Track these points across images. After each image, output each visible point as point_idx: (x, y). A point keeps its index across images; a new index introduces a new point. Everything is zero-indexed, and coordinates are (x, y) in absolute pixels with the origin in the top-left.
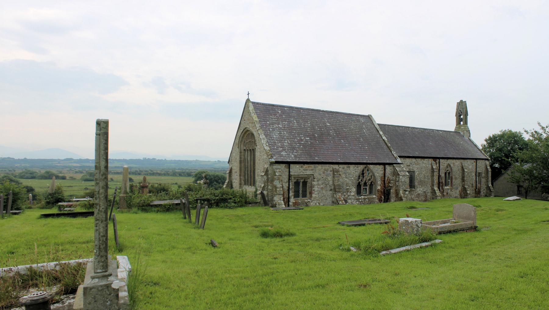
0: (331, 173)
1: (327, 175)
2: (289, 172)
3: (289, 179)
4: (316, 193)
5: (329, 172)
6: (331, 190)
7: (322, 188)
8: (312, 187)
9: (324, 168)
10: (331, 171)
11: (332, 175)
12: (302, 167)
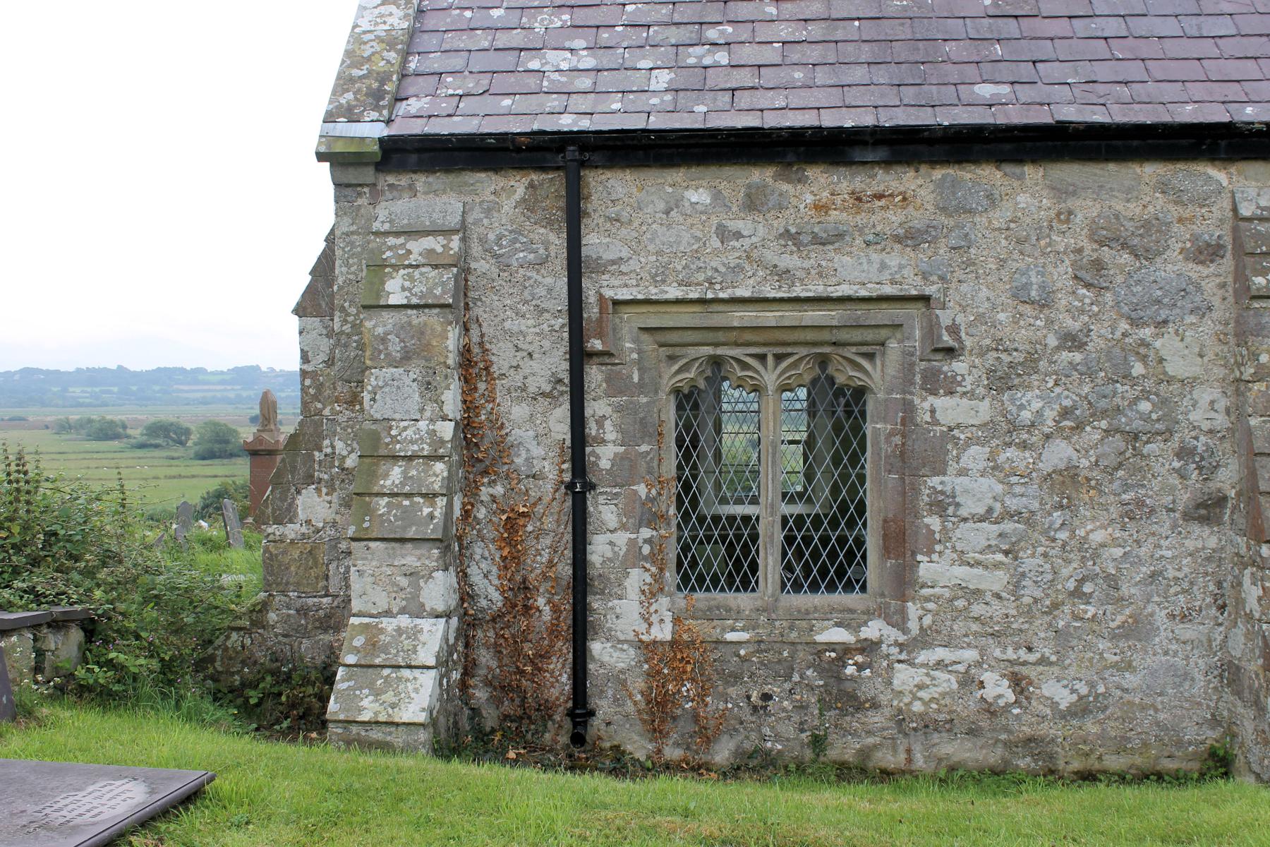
0: (1212, 279)
1: (1149, 313)
2: (575, 266)
3: (579, 356)
4: (974, 537)
5: (1172, 266)
6: (1208, 510)
7: (1066, 482)
8: (922, 454)
9: (1086, 209)
10: (1207, 253)
11: (1222, 310)
12: (752, 203)
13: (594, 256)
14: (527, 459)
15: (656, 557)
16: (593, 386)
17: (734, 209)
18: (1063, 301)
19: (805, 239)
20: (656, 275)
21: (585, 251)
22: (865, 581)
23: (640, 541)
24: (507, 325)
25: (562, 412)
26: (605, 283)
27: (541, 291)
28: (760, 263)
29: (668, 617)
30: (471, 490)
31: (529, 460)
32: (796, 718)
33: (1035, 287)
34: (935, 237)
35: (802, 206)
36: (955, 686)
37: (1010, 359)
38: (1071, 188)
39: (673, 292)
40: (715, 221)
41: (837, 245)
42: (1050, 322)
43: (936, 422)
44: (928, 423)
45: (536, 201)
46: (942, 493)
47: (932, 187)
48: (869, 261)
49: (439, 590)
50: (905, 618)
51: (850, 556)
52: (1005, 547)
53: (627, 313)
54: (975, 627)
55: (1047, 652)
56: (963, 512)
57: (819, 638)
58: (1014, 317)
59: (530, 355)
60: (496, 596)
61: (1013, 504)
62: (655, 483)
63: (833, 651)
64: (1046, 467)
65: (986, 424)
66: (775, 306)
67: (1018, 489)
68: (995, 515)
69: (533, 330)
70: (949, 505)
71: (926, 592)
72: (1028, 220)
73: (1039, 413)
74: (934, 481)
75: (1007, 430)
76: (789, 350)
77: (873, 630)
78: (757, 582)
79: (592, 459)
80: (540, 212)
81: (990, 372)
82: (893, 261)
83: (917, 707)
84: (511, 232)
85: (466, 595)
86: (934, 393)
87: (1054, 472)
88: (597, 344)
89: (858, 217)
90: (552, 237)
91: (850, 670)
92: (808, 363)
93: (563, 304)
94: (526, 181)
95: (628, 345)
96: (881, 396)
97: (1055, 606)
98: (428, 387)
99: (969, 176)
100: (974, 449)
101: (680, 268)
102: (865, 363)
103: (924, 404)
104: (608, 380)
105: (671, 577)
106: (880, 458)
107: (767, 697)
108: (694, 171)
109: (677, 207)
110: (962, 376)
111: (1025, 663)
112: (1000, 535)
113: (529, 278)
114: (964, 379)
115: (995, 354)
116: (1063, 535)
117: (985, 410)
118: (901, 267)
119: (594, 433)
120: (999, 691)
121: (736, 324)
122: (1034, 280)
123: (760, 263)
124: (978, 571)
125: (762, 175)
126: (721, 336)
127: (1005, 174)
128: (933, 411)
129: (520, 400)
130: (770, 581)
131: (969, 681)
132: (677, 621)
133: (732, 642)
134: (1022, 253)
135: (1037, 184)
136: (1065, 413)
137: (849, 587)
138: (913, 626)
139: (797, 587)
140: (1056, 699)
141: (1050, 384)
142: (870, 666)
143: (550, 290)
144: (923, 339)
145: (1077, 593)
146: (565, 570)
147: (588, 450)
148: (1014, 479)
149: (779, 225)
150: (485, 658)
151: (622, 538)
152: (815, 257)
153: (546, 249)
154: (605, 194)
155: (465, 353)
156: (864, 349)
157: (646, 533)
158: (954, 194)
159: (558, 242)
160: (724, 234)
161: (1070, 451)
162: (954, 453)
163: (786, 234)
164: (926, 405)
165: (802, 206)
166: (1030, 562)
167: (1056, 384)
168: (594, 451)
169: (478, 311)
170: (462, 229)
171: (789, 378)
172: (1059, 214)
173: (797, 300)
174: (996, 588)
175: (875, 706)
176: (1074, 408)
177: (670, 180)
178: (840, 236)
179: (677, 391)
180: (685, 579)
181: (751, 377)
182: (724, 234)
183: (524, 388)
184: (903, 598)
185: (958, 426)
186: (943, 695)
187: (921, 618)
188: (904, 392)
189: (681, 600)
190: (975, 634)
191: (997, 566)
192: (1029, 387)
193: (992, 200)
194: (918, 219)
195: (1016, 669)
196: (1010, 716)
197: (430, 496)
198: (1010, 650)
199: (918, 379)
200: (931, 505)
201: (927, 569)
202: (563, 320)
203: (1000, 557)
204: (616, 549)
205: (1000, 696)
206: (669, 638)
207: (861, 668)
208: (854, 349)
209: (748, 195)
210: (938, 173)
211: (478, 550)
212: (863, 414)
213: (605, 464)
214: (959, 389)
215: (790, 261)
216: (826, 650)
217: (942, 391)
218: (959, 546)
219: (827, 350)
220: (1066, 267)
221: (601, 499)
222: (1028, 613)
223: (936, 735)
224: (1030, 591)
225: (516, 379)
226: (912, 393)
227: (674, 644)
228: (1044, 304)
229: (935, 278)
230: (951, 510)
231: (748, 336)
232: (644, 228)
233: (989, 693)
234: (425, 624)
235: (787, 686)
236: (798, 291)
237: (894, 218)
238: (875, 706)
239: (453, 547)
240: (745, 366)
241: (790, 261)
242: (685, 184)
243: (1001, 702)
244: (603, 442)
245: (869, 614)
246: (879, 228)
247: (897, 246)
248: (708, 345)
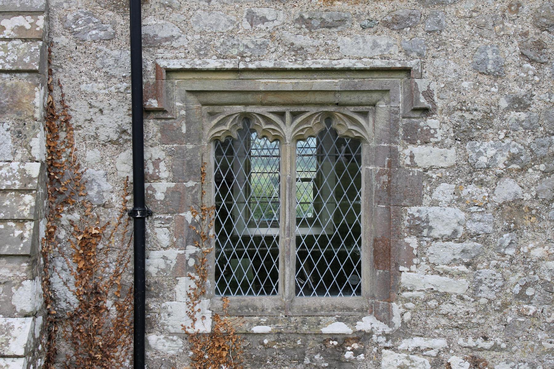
2: (137, 42)
3: (139, 112)
7: (513, 211)
8: (404, 189)
15: (199, 268)
18: (512, 73)
29: (208, 314)
30: (53, 216)
31: (100, 193)
39: (213, 64)
42: (502, 89)
49: (27, 295)
50: (390, 315)
51: (349, 267)
53: (177, 79)
60: (73, 299)
61: (473, 227)
64: (498, 199)
74: (413, 210)
77: (366, 323)
81: (456, 127)
82: (383, 41)
85: (49, 298)
88: (153, 103)
91: (349, 355)
93: (127, 71)
97: (505, 305)
98: (20, 136)
103: (406, 151)
105: (211, 283)
129: (93, 146)
132: (215, 317)
136: (513, 158)
137: (347, 291)
138: (397, 320)
139: (308, 291)
145: (521, 296)
146: (128, 279)
149: (295, 12)
150: (65, 348)
151: (173, 254)
152: (323, 37)
155: (49, 108)
157: (192, 249)
159: (123, 23)
160: (252, 18)
169: (59, 76)
170: (47, 11)
178: (342, 21)
179: (216, 140)
180: (222, 285)
182: (252, 18)
189: (218, 301)
191: (461, 275)
192: (485, 139)
197: (21, 221)
201: (407, 277)
202: (127, 84)
207: (356, 353)
211: (59, 263)
213: (160, 196)
215: (303, 40)
222: (484, 311)
224: (485, 294)
225: (91, 129)
227: (213, 335)
228: (498, 75)
234: (16, 322)
236: (310, 64)
239: (39, 261)
240: (268, 121)
241: (303, 40)
245: (363, 311)
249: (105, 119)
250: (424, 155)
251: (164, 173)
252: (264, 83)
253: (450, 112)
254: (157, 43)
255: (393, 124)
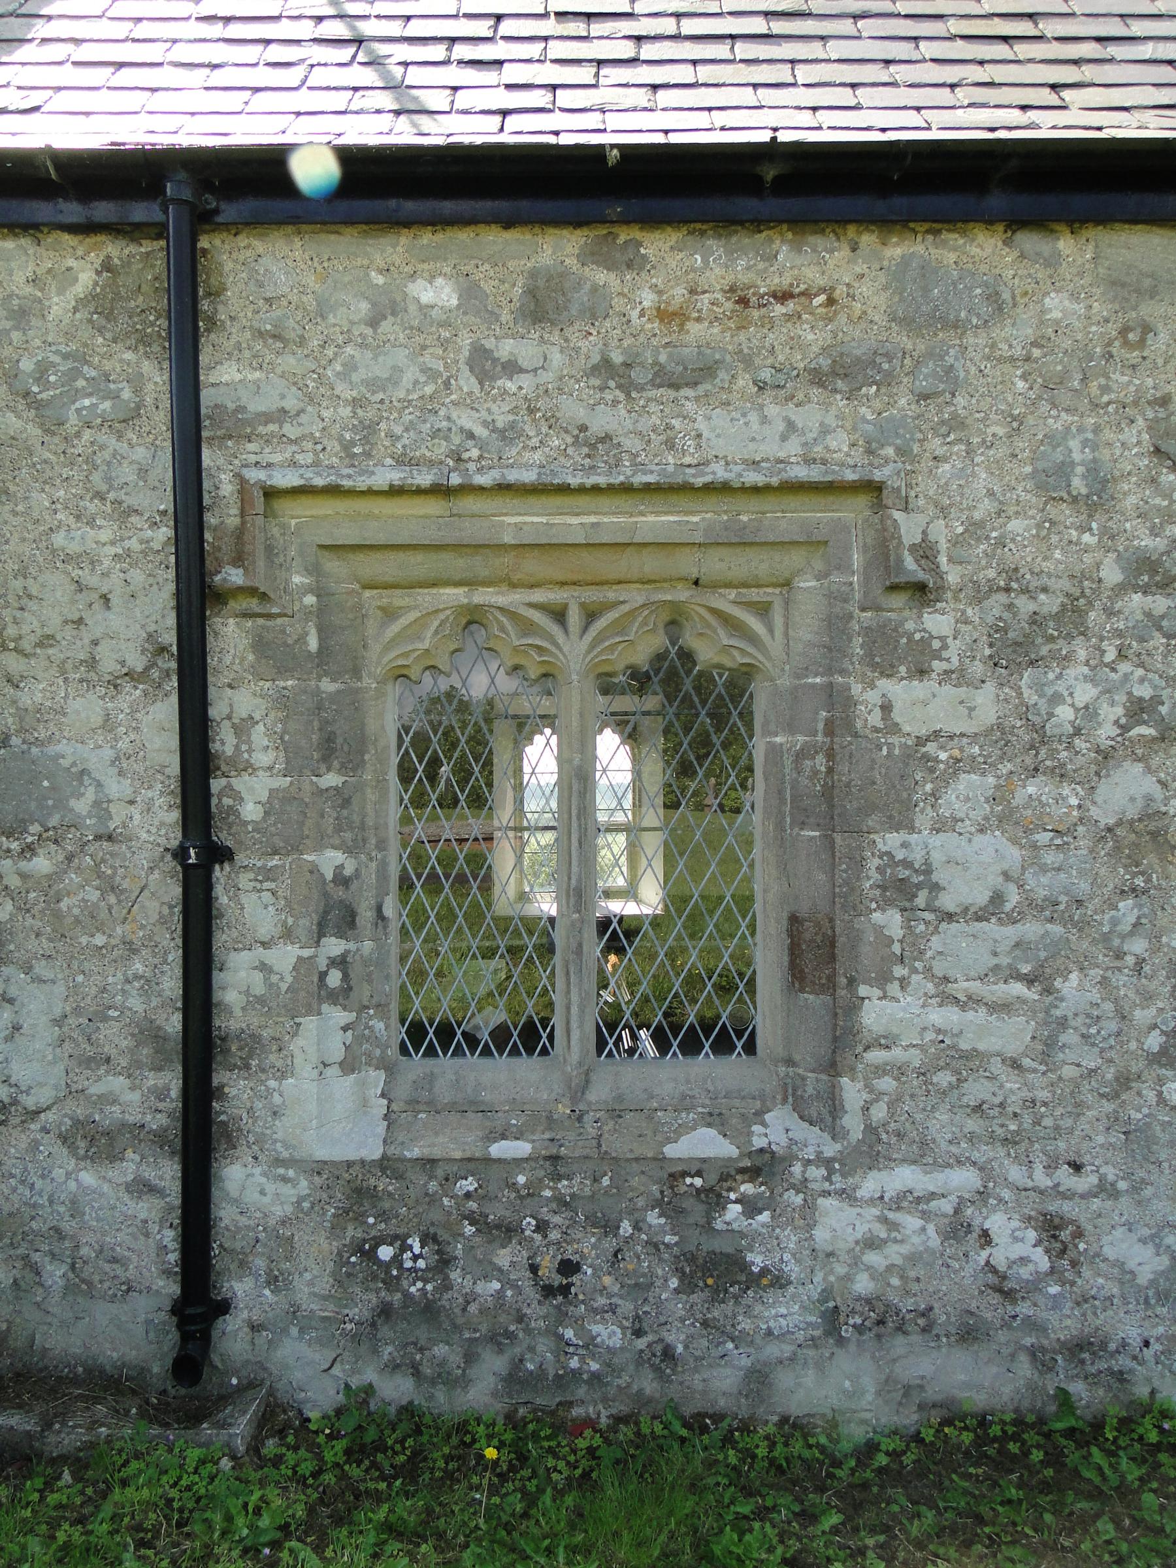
3: (197, 597)
12: (542, 306)
13: (231, 406)
14: (97, 804)
16: (228, 660)
17: (505, 316)
19: (639, 376)
20: (353, 443)
21: (207, 397)
22: (753, 1033)
23: (322, 964)
24: (59, 539)
25: (163, 714)
26: (253, 458)
27: (127, 473)
28: (552, 421)
32: (626, 1307)
33: (1080, 470)
34: (889, 374)
35: (635, 314)
36: (935, 1241)
37: (1032, 607)
38: (1147, 282)
40: (465, 341)
41: (701, 389)
42: (1109, 535)
43: (894, 728)
44: (876, 730)
45: (117, 297)
46: (907, 864)
47: (882, 278)
48: (764, 420)
50: (834, 1106)
52: (1025, 969)
53: (295, 513)
54: (973, 1124)
55: (1110, 1172)
56: (947, 902)
57: (670, 1151)
58: (1039, 526)
59: (105, 598)
61: (1041, 885)
62: (367, 855)
63: (699, 1174)
65: (989, 731)
66: (583, 501)
67: (1050, 858)
68: (1008, 907)
69: (112, 550)
70: (919, 886)
71: (876, 1056)
72: (1067, 343)
73: (1089, 712)
74: (891, 841)
75: (1031, 744)
76: (611, 594)
77: (777, 1129)
78: (551, 1037)
79: (227, 801)
80: (123, 319)
82: (809, 417)
83: (863, 1285)
84: (66, 356)
86: (888, 672)
87: (1120, 823)
88: (234, 576)
89: (742, 337)
90: (147, 367)
92: (645, 623)
94: (95, 258)
95: (297, 579)
96: (785, 682)
97: (1124, 1081)
99: (952, 257)
100: (967, 782)
101: (398, 430)
102: (755, 624)
104: (260, 645)
106: (782, 801)
107: (568, 1268)
108: (428, 238)
109: (394, 314)
110: (942, 639)
111: (1068, 1195)
112: (1017, 945)
113: (102, 447)
114: (945, 647)
115: (1002, 598)
116: (1138, 946)
117: (987, 704)
118: (825, 431)
119: (229, 750)
120: (1019, 1250)
121: (508, 539)
122: (1077, 456)
123: (552, 421)
124: (980, 1015)
125: (557, 250)
126: (479, 565)
127: (1022, 256)
128: (886, 708)
130: (575, 1035)
131: (958, 1229)
133: (499, 1161)
134: (1054, 406)
135: (1081, 274)
136: (1139, 710)
138: (853, 1124)
140: (1131, 1265)
141: (1111, 655)
142: (770, 1204)
143: (143, 472)
144: (867, 567)
147: (216, 785)
148: (1043, 838)
149: (590, 347)
151: (1077, 1454)
152: (655, 410)
153: (137, 391)
154: (252, 287)
156: (754, 594)
158: (926, 291)
159: (157, 378)
160: (484, 365)
161: (1149, 785)
162: (929, 787)
163: (604, 368)
164: (873, 697)
165: (635, 314)
166: (1073, 988)
167: (1122, 655)
168: (229, 786)
171: (612, 648)
172: (1124, 331)
173: (626, 489)
174: (1013, 1049)
175: (780, 1282)
176: (1157, 700)
177: (380, 262)
181: (538, 647)
182: (484, 365)
183: (92, 663)
184: (832, 1068)
185: (937, 734)
186: (913, 1259)
187: (866, 1109)
188: (829, 671)
190: (972, 1138)
193: (998, 305)
194: (858, 340)
195: (1053, 1207)
196: (1041, 1301)
198: (1039, 1171)
199: (857, 646)
200: (883, 888)
201: (876, 1013)
203: (1018, 988)
204: (274, 978)
205: (1024, 1261)
206: (377, 1155)
207: (751, 1207)
208: (732, 594)
209: (531, 292)
210: (898, 249)
212: (747, 717)
213: (251, 811)
214: (936, 664)
215: (608, 419)
216: (684, 1174)
217: (903, 669)
218: (939, 969)
219: (682, 594)
220: (1137, 435)
221: (245, 880)
223: (900, 1340)
224: (1076, 1057)
226: (843, 672)
229: (890, 451)
230: (921, 900)
231: (532, 566)
232: (330, 352)
233: (1001, 1255)
235: (610, 1244)
237: (811, 337)
238: (780, 1282)
240: (528, 627)
242: (408, 269)
243: (1025, 1272)
244: (249, 768)
246: (781, 358)
247: (815, 391)
248: (457, 584)
249: (115, 620)
250: (917, 705)
251: (262, 759)
252: (521, 521)
253: (980, 594)
254: (241, 427)
255: (836, 626)
